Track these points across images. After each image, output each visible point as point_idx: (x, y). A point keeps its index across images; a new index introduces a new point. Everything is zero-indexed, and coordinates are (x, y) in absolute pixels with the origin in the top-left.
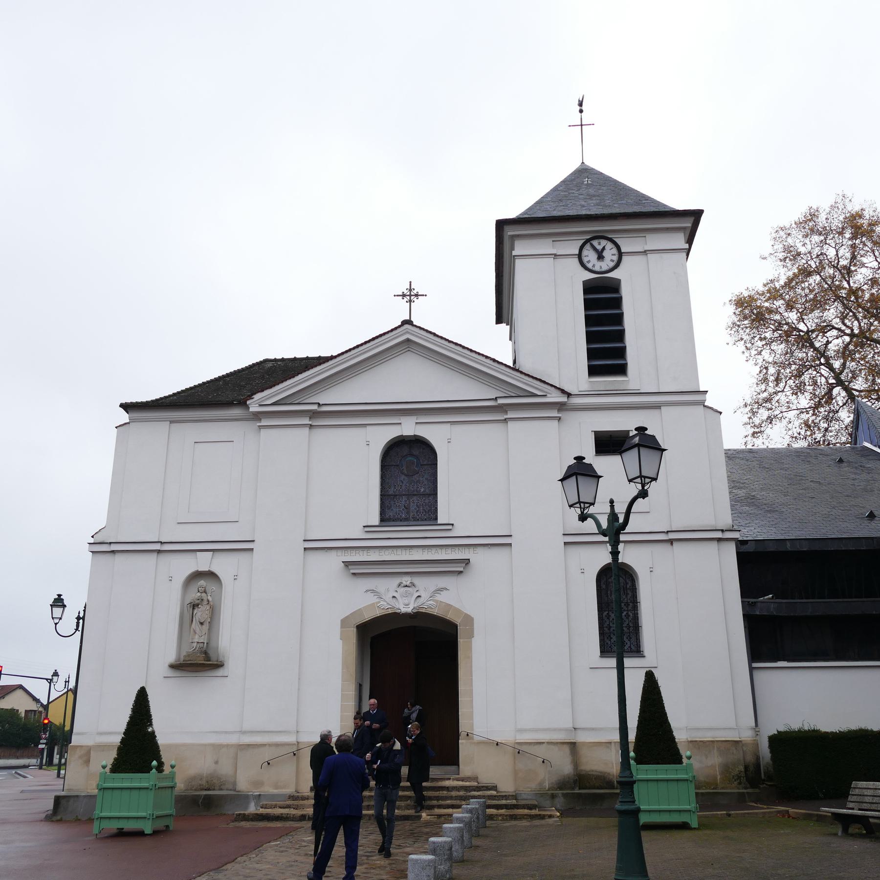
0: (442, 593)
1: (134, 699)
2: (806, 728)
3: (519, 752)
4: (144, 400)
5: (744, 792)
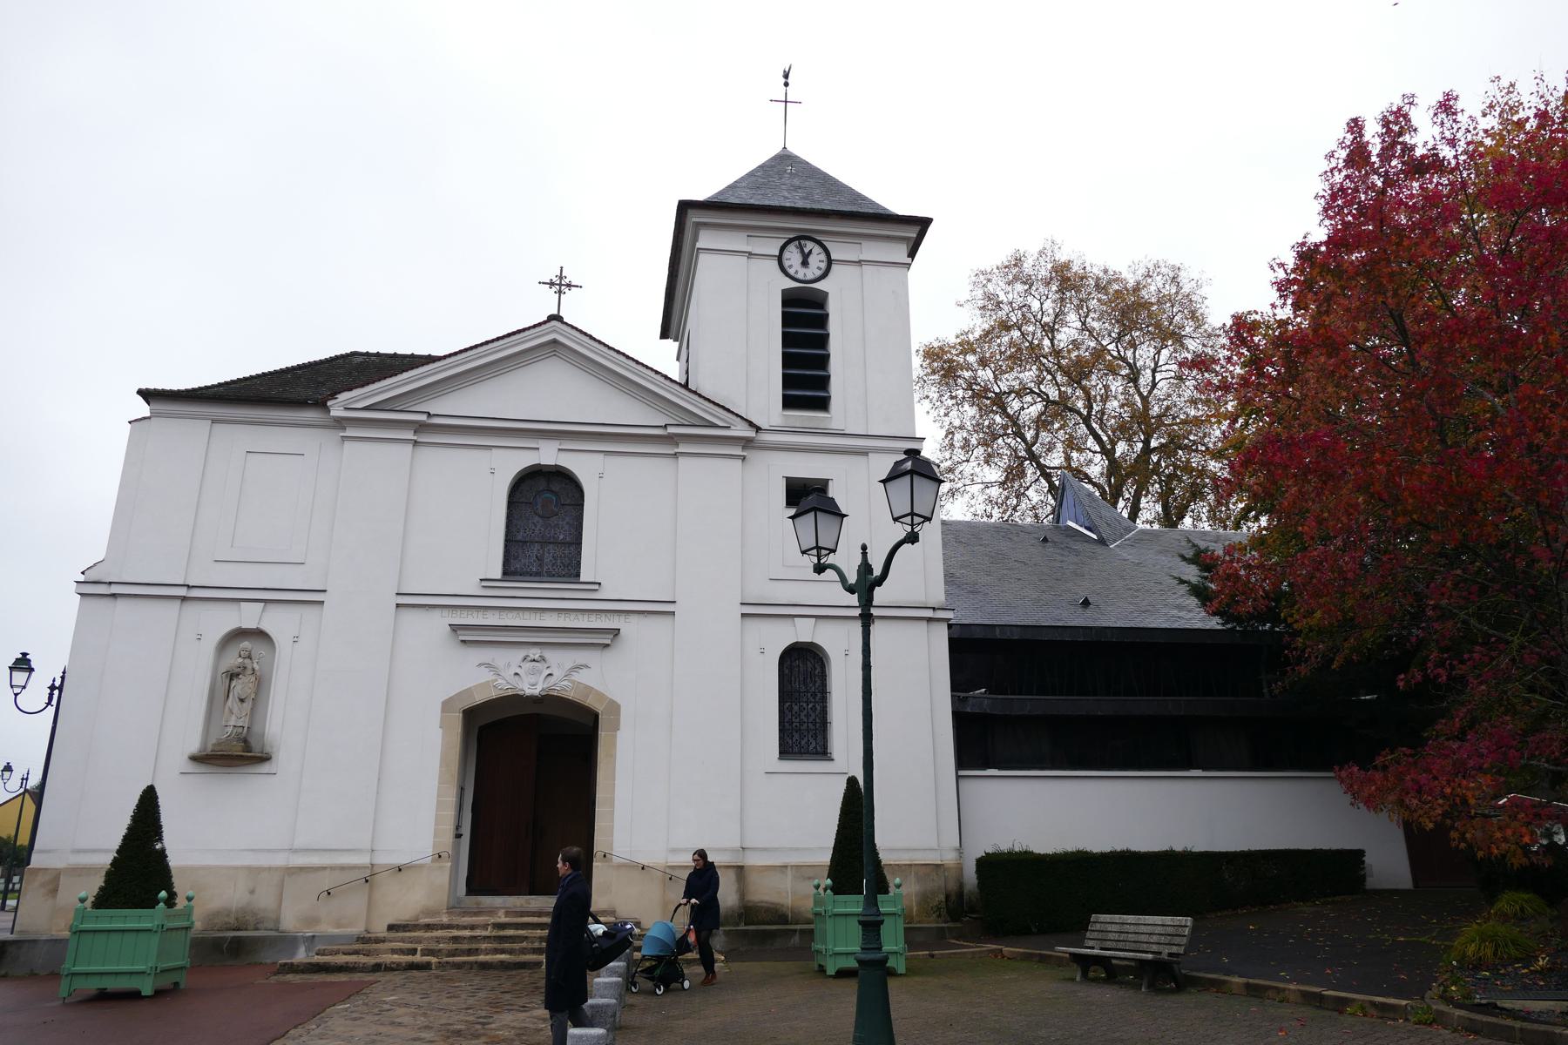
0: (580, 671)
1: (137, 802)
2: (1017, 849)
3: (670, 879)
4: (175, 388)
5: (943, 927)
